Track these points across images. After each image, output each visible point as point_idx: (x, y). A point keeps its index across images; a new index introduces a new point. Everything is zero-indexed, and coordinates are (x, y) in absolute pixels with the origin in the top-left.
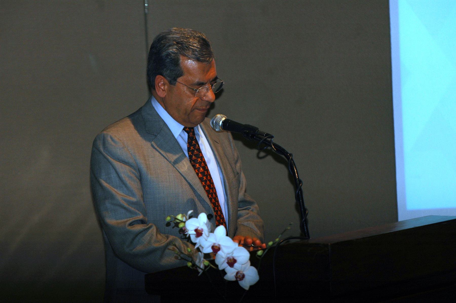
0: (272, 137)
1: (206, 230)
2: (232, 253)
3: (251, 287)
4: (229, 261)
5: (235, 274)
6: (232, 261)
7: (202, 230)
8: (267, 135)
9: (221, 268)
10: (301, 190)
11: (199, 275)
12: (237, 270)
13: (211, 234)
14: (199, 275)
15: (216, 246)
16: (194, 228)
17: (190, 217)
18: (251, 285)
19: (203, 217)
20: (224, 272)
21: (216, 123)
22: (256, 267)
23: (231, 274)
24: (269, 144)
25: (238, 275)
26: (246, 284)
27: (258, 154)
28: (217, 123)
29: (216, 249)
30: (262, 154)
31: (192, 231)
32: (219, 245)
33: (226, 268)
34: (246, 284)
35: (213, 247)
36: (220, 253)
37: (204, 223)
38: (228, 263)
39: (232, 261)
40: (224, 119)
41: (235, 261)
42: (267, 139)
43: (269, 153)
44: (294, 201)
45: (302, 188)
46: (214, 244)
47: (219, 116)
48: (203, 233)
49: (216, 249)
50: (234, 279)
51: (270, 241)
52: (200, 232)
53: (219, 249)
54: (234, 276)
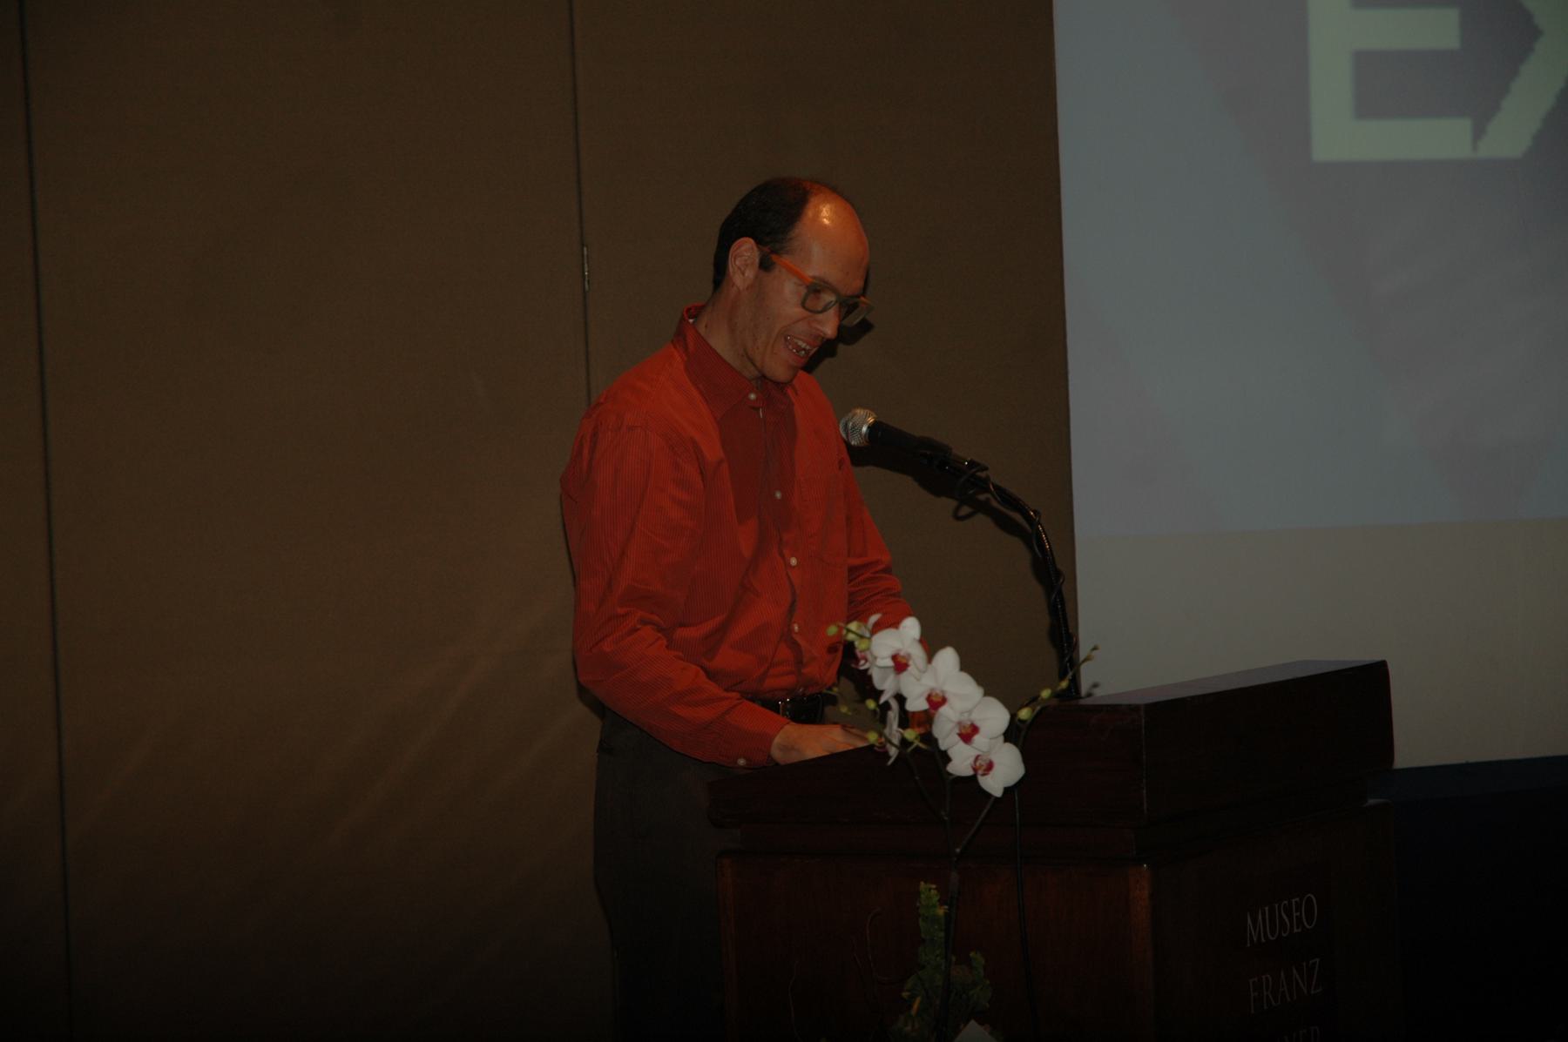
0: (986, 469)
1: (917, 653)
2: (970, 712)
3: (1008, 791)
4: (963, 731)
5: (972, 760)
6: (969, 731)
7: (909, 656)
8: (972, 464)
9: (943, 746)
10: (1060, 593)
11: (890, 762)
12: (979, 750)
13: (929, 666)
14: (890, 762)
15: (937, 695)
16: (890, 652)
17: (878, 627)
18: (1007, 785)
19: (911, 627)
20: (946, 758)
21: (853, 427)
22: (1016, 744)
23: (961, 761)
24: (983, 485)
25: (978, 764)
26: (995, 784)
27: (957, 509)
28: (856, 428)
29: (936, 702)
30: (965, 510)
31: (883, 658)
32: (943, 691)
33: (952, 747)
34: (995, 784)
35: (929, 699)
36: (944, 710)
37: (914, 639)
38: (961, 735)
39: (969, 731)
40: (871, 420)
41: (975, 729)
42: (979, 474)
43: (984, 508)
44: (1045, 620)
45: (1064, 589)
46: (932, 689)
47: (860, 412)
48: (911, 663)
49: (936, 702)
50: (970, 772)
51: (1045, 687)
52: (904, 661)
53: (944, 701)
54: (970, 766)
